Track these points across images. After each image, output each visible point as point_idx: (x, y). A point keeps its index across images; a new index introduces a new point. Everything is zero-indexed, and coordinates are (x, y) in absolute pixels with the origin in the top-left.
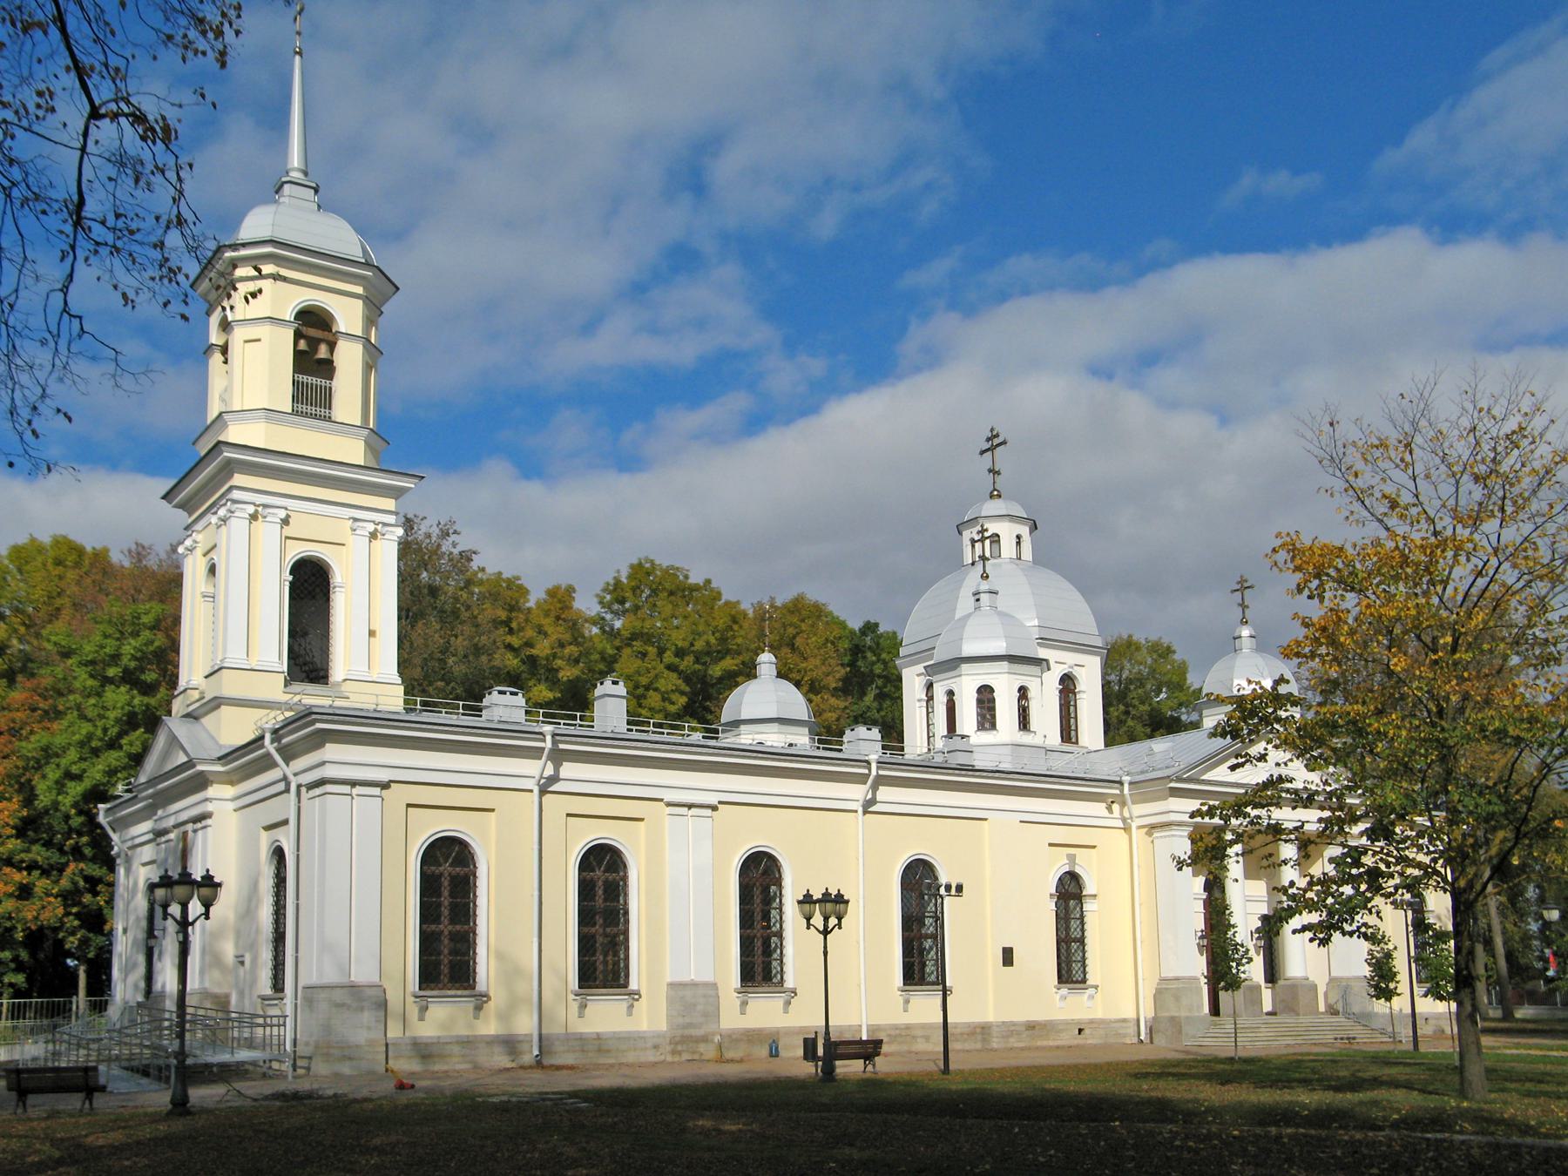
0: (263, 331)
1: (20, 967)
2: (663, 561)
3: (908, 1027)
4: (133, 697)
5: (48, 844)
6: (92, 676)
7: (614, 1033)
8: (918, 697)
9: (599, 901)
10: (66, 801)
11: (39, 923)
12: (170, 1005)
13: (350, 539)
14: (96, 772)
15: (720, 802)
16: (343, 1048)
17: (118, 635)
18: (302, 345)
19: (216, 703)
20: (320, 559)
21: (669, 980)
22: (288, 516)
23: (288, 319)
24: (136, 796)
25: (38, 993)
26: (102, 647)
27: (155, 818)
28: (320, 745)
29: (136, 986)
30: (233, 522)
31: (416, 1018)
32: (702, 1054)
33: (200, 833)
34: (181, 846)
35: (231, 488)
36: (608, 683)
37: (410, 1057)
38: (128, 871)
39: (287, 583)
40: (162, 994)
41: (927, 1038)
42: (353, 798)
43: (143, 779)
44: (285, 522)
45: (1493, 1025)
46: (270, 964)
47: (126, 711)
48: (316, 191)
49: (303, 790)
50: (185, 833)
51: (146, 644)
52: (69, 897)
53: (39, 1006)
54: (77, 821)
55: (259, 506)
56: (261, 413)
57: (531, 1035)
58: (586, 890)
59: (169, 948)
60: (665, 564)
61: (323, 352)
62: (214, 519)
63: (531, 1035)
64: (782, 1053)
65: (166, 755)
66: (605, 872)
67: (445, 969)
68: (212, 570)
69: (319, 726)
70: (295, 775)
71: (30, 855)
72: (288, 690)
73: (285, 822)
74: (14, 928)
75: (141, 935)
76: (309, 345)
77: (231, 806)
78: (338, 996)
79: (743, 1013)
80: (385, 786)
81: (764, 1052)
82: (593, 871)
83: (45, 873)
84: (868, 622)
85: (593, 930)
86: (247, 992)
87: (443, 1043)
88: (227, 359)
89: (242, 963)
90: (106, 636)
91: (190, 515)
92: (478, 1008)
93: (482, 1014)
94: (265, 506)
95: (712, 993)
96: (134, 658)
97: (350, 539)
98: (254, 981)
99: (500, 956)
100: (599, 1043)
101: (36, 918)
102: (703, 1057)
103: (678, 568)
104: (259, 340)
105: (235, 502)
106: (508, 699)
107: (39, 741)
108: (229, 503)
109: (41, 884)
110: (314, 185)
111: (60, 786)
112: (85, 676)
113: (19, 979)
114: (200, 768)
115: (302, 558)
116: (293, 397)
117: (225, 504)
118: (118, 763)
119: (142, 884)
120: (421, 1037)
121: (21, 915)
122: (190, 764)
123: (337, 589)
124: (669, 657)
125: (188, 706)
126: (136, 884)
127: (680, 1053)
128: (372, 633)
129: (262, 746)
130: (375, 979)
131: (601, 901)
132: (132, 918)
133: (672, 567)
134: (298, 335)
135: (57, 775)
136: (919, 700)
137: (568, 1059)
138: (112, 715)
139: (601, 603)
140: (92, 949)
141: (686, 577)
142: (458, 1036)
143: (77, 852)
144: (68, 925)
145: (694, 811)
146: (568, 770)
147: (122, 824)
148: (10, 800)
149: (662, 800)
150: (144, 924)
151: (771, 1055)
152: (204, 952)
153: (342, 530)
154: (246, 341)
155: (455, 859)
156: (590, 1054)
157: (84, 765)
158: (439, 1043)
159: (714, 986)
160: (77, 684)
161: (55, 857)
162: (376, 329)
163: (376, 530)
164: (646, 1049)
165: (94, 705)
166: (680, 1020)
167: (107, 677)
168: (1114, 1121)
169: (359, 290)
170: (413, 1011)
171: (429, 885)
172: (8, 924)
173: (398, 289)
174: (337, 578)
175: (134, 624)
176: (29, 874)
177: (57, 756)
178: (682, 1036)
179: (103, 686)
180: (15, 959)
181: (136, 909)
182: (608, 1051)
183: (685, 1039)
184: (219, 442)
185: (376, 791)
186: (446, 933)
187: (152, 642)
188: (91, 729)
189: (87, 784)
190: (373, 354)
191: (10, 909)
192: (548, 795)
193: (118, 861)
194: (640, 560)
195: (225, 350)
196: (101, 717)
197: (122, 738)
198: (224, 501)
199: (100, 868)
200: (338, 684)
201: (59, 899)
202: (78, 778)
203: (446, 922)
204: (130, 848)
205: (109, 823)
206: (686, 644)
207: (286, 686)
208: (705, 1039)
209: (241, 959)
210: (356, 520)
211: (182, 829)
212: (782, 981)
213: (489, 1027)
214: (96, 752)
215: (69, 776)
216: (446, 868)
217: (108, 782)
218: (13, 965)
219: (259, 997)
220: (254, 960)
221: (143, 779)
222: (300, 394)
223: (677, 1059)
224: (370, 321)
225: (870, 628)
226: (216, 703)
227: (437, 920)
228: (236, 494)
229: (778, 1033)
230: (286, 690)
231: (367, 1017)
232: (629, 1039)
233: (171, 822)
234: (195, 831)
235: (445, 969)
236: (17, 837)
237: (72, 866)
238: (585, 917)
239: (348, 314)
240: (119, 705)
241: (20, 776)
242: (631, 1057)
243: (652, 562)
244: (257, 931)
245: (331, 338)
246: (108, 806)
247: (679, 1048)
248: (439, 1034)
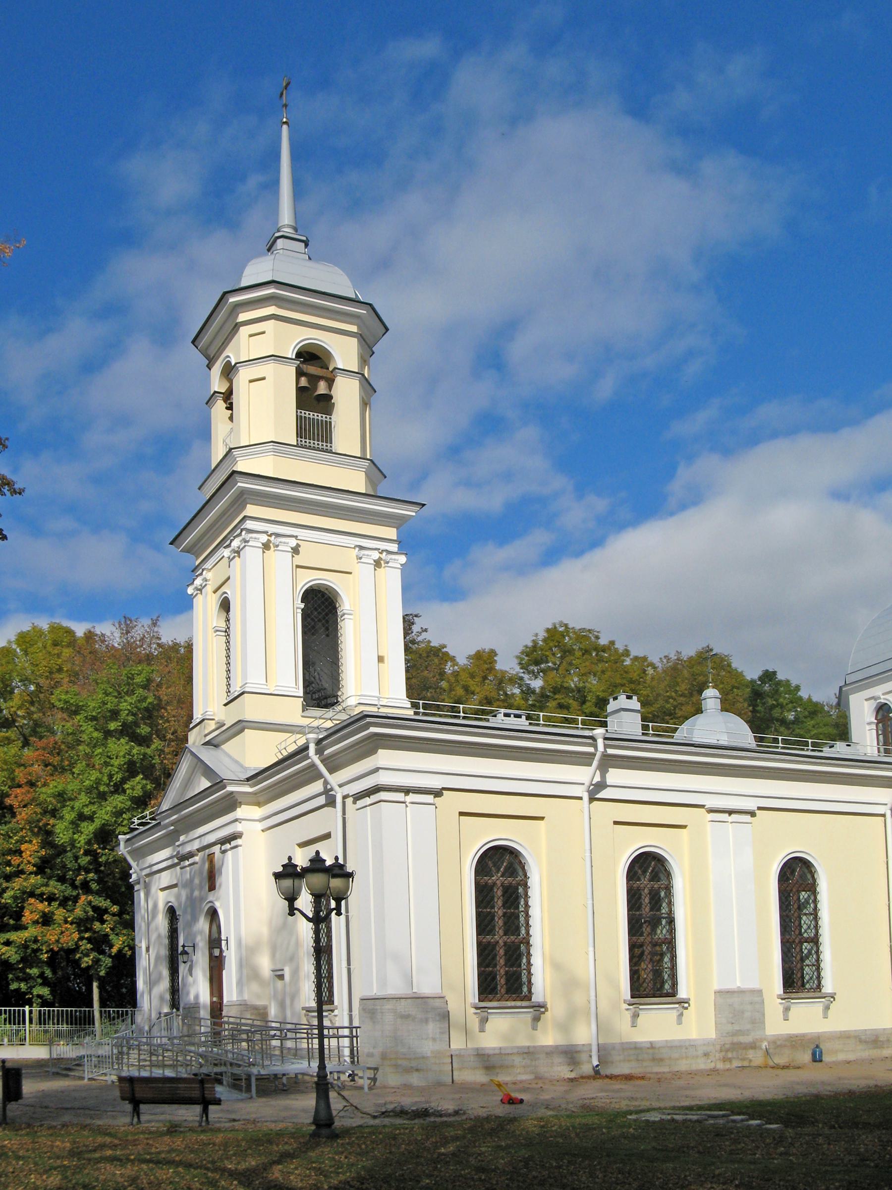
0: (268, 369)
1: (46, 982)
2: (577, 623)
4: (132, 748)
5: (62, 879)
6: (96, 730)
7: (666, 1041)
8: (868, 720)
9: (646, 910)
10: (80, 839)
11: (60, 945)
12: (205, 1013)
13: (356, 568)
14: (104, 814)
15: (759, 808)
16: (410, 1059)
17: (116, 694)
18: (304, 382)
19: (240, 727)
20: (329, 588)
21: (716, 987)
22: (298, 545)
23: (290, 356)
24: (160, 823)
25: (59, 1003)
26: (104, 703)
27: (177, 843)
28: (372, 752)
29: (161, 998)
30: (248, 552)
31: (478, 1030)
32: (750, 1061)
33: (229, 853)
34: (207, 866)
35: (245, 518)
36: (622, 697)
37: (475, 1068)
38: (147, 895)
39: (300, 611)
40: (196, 1006)
42: (407, 806)
43: (165, 806)
44: (296, 550)
46: (313, 978)
47: (126, 760)
48: (307, 245)
49: (349, 801)
50: (211, 856)
51: (139, 701)
52: (83, 924)
53: (44, 1013)
54: (84, 860)
55: (270, 536)
56: (270, 446)
57: (590, 1045)
59: (200, 961)
60: (578, 627)
61: (322, 388)
62: (227, 553)
63: (590, 1045)
64: (826, 1058)
65: (188, 782)
66: (650, 881)
68: (225, 605)
69: (373, 730)
70: (340, 786)
71: (49, 889)
72: (305, 714)
73: (327, 836)
74: (39, 950)
75: (164, 952)
76: (309, 382)
77: (260, 826)
78: (403, 1006)
79: (786, 1019)
80: (438, 793)
81: (807, 1057)
82: (639, 880)
84: (767, 671)
85: (642, 938)
86: (288, 1002)
87: (505, 1054)
88: (231, 404)
89: (281, 977)
90: (107, 694)
91: (197, 558)
92: (536, 1019)
93: (539, 1024)
94: (277, 535)
95: (757, 999)
96: (130, 713)
97: (356, 568)
98: (294, 996)
99: (557, 966)
100: (652, 1052)
101: (58, 941)
102: (753, 1064)
103: (589, 631)
104: (264, 379)
107: (56, 787)
108: (244, 533)
109: (59, 914)
110: (304, 238)
111: (75, 825)
112: (91, 730)
113: (45, 991)
114: (230, 788)
115: (311, 587)
116: (297, 434)
117: (240, 534)
118: (123, 805)
119: (161, 906)
120: (483, 1049)
121: (45, 939)
122: (222, 781)
123: (346, 616)
125: (206, 736)
126: (155, 906)
127: (730, 1060)
128: (381, 659)
129: (307, 757)
131: (647, 909)
132: (153, 937)
133: (583, 630)
134: (300, 373)
135: (73, 817)
136: (869, 724)
137: (624, 1069)
138: (116, 762)
139: (520, 664)
140: (102, 968)
141: (597, 638)
142: (518, 1047)
143: (85, 887)
144: (83, 948)
145: (735, 817)
147: (141, 853)
148: (30, 842)
149: (702, 806)
150: (166, 941)
151: (814, 1060)
152: (240, 966)
153: (347, 558)
154: (251, 381)
155: (506, 869)
156: (645, 1064)
157: (93, 808)
158: (501, 1054)
159: (759, 992)
160: (85, 737)
161: (70, 892)
162: (369, 368)
163: (380, 559)
164: (697, 1057)
165: (100, 753)
166: (730, 1028)
167: (109, 731)
169: (354, 329)
170: (474, 1021)
171: (483, 894)
172: (35, 947)
173: (387, 329)
174: (346, 604)
175: (128, 684)
176: (49, 905)
177: (70, 799)
178: (733, 1044)
179: (106, 738)
180: (42, 975)
181: (157, 928)
182: (662, 1060)
183: (737, 1047)
184: (234, 472)
185: (429, 798)
186: (501, 943)
187: (146, 698)
188: (100, 776)
189: (97, 823)
190: (368, 389)
191: (35, 934)
192: (595, 802)
193: (136, 888)
194: (554, 625)
195: (228, 396)
196: (106, 764)
197: (125, 783)
198: (239, 531)
199: (105, 900)
201: (74, 925)
202: (91, 818)
203: (501, 932)
204: (148, 875)
205: (129, 852)
207: (303, 711)
208: (753, 1046)
209: (280, 973)
210: (361, 548)
211: (207, 851)
212: (819, 987)
213: (548, 1037)
214: (103, 796)
215: (82, 817)
216: (497, 879)
217: (115, 821)
218: (40, 981)
219: (303, 1009)
220: (296, 972)
221: (165, 806)
222: (304, 430)
223: (728, 1066)
225: (768, 676)
226: (240, 727)
228: (249, 524)
229: (819, 1037)
230: (303, 714)
231: (432, 1028)
232: (681, 1047)
233: (196, 845)
234: (224, 852)
236: (36, 874)
237: (83, 898)
240: (122, 754)
241: (39, 821)
242: (683, 1066)
243: (566, 625)
244: (297, 944)
245: (329, 376)
246: (128, 836)
247: (730, 1055)
248: (501, 1045)
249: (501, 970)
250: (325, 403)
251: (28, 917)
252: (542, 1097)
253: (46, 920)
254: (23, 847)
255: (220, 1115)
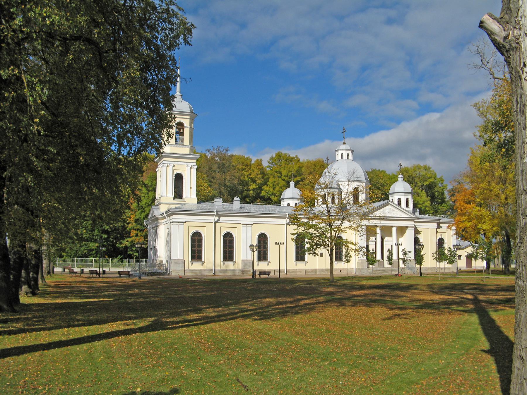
3: (297, 269)
13: (187, 169)
41: (301, 272)
44: (174, 166)
45: (84, 279)
58: (225, 242)
61: (181, 131)
67: (196, 257)
80: (185, 222)
83: (140, 231)
105: (164, 164)
106: (219, 200)
109: (140, 234)
124: (283, 177)
128: (191, 188)
130: (182, 258)
146: (222, 218)
168: (10, 278)
169: (189, 117)
185: (183, 223)
200: (184, 199)
206: (287, 174)
224: (191, 123)
227: (195, 247)
228: (164, 162)
235: (196, 257)
238: (224, 247)
239: (186, 122)
249: (196, 254)
250: (182, 134)
251: (132, 235)
252: (333, 288)
253: (137, 235)
254: (131, 216)
255: (317, 306)
